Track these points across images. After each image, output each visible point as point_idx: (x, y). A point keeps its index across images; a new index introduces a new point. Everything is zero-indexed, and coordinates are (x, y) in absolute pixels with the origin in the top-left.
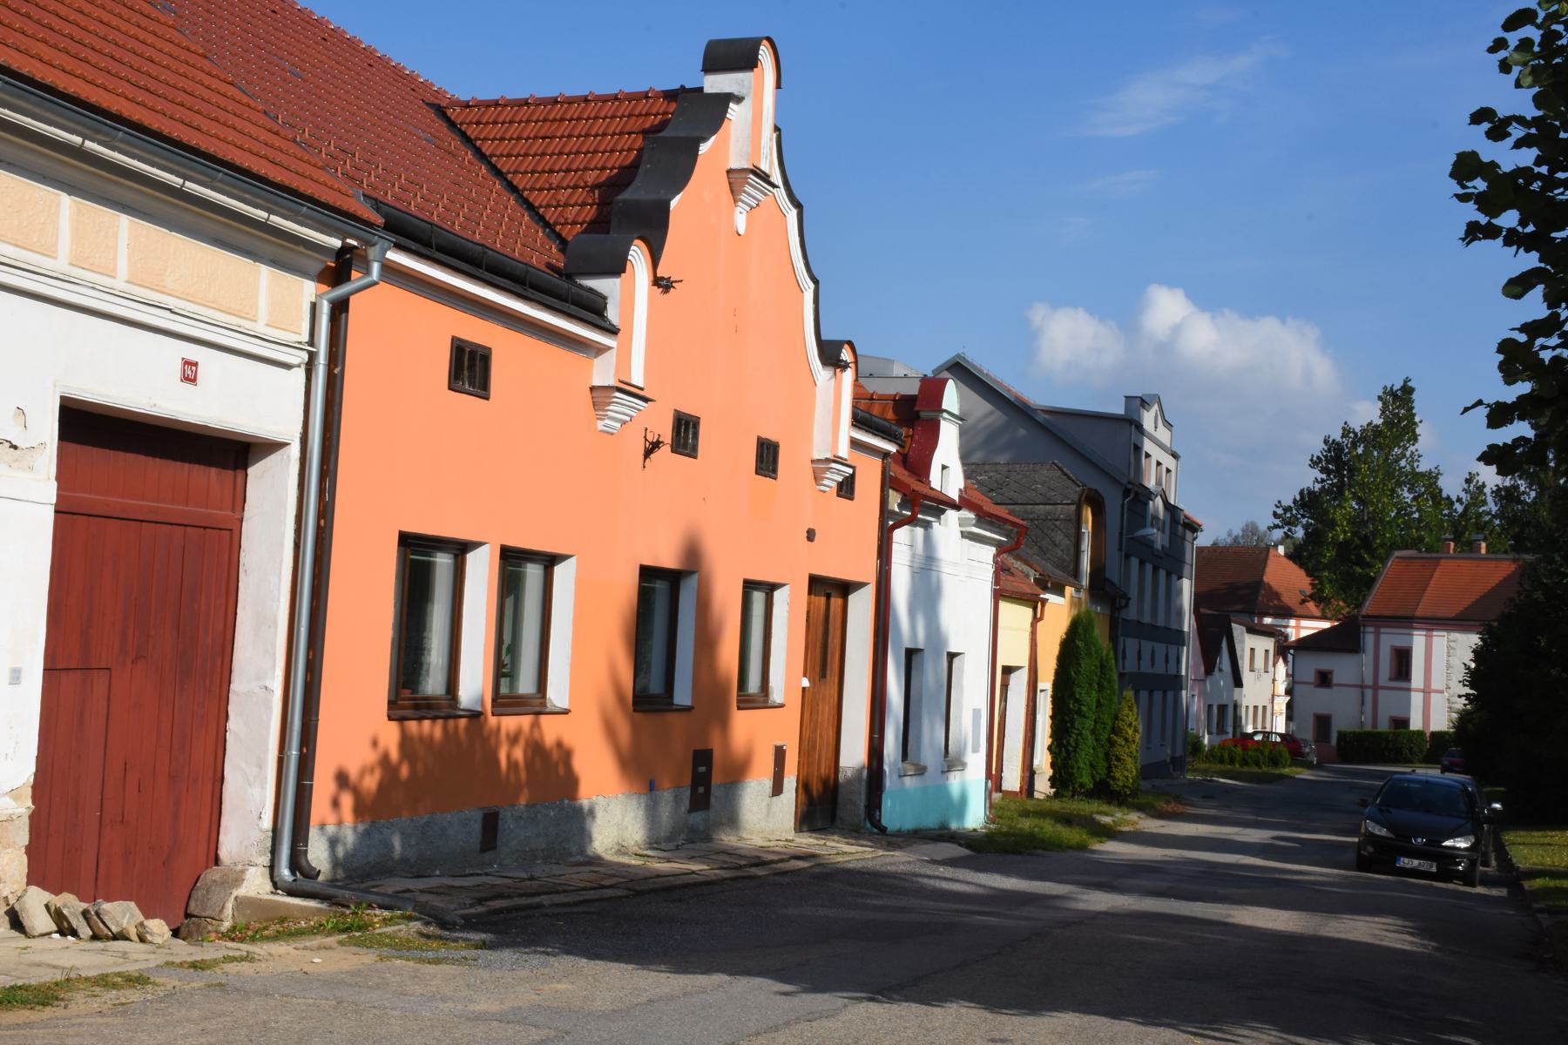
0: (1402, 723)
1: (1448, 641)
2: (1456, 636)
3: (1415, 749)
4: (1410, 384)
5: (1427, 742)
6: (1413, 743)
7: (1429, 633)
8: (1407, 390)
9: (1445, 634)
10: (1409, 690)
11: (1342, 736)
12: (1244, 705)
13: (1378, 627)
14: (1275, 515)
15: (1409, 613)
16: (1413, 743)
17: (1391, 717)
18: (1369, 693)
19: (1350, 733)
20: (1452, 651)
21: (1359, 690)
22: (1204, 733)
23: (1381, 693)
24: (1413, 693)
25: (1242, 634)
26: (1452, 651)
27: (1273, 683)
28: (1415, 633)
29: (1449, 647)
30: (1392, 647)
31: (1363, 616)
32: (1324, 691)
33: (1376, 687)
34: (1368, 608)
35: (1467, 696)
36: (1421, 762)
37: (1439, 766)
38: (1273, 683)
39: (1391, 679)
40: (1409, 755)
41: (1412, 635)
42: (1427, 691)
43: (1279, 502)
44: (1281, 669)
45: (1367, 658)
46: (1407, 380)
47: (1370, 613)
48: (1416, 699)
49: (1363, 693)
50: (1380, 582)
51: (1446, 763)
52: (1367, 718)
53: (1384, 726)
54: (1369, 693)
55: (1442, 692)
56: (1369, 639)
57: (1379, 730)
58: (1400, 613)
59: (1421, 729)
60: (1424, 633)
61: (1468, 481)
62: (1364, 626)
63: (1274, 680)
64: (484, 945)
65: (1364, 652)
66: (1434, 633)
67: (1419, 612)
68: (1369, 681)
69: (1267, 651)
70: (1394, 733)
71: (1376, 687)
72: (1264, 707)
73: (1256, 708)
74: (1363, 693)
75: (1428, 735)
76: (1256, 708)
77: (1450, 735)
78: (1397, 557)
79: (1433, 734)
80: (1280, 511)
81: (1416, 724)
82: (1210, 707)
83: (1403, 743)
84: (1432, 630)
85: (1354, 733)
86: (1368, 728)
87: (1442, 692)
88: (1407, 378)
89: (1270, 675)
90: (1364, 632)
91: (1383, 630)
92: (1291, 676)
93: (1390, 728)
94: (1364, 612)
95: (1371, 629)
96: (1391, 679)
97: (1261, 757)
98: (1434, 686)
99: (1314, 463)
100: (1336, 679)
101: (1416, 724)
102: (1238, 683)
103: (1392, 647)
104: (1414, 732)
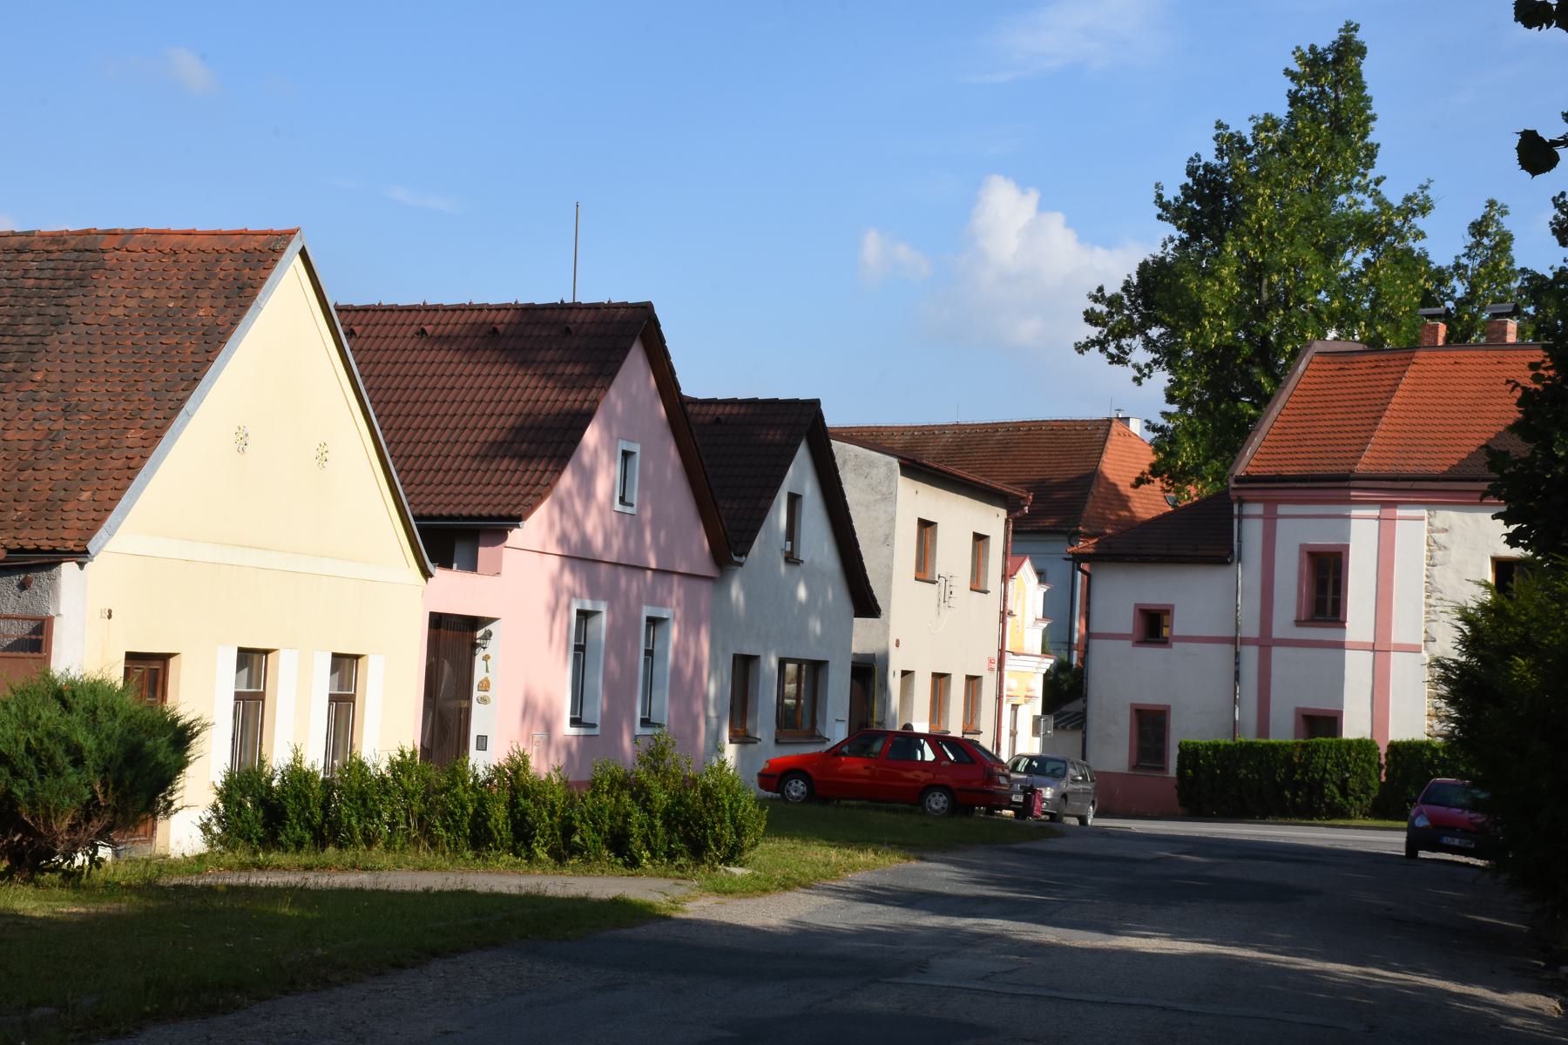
0: (1324, 723)
1: (1431, 531)
2: (1448, 517)
3: (1353, 783)
4: (1359, 37)
5: (1380, 767)
6: (1347, 769)
7: (1388, 512)
8: (1348, 50)
9: (1423, 512)
10: (1340, 646)
11: (1189, 754)
12: (896, 666)
13: (1271, 504)
14: (1091, 318)
15: (1342, 469)
16: (1347, 769)
17: (1298, 710)
18: (1251, 655)
19: (1207, 747)
20: (1439, 554)
21: (1229, 648)
22: (717, 736)
23: (1276, 652)
24: (1347, 651)
25: (889, 478)
26: (1439, 554)
27: (1003, 621)
28: (1355, 512)
29: (1433, 544)
30: (1302, 547)
31: (1239, 480)
32: (1151, 655)
33: (1266, 642)
34: (1249, 460)
35: (1455, 720)
36: (1365, 815)
37: (1404, 824)
38: (1003, 621)
39: (1299, 623)
40: (1339, 799)
41: (1349, 517)
42: (1380, 649)
43: (1100, 289)
44: (1028, 592)
45: (1247, 574)
46: (1350, 28)
47: (1254, 471)
48: (1357, 667)
49: (1237, 654)
50: (1279, 406)
51: (1421, 822)
52: (1246, 714)
53: (1283, 732)
54: (1251, 655)
55: (1416, 649)
56: (1251, 532)
57: (1272, 740)
58: (1320, 470)
59: (1368, 737)
60: (1376, 512)
61: (1478, 229)
62: (1241, 502)
63: (1004, 614)
64: (855, 900)
65: (1239, 560)
66: (1400, 512)
67: (1360, 468)
68: (1251, 629)
69: (979, 539)
70: (1305, 746)
71: (1266, 642)
72: (973, 681)
73: (940, 679)
74: (1237, 654)
75: (1383, 751)
76: (940, 680)
77: (1435, 750)
78: (1319, 353)
79: (1394, 748)
80: (1101, 308)
81: (1355, 727)
82: (744, 666)
83: (1325, 770)
84: (1394, 504)
85: (1216, 748)
86: (1248, 735)
87: (1416, 649)
88: (1348, 24)
89: (993, 601)
90: (1241, 517)
91: (1282, 509)
92: (1058, 615)
93: (1297, 736)
94: (1240, 470)
95: (1257, 509)
96: (1299, 623)
97: (637, 815)
98: (1397, 637)
99: (1170, 211)
100: (1180, 625)
101: (1355, 727)
102: (865, 603)
103: (1302, 547)
104: (1350, 744)
